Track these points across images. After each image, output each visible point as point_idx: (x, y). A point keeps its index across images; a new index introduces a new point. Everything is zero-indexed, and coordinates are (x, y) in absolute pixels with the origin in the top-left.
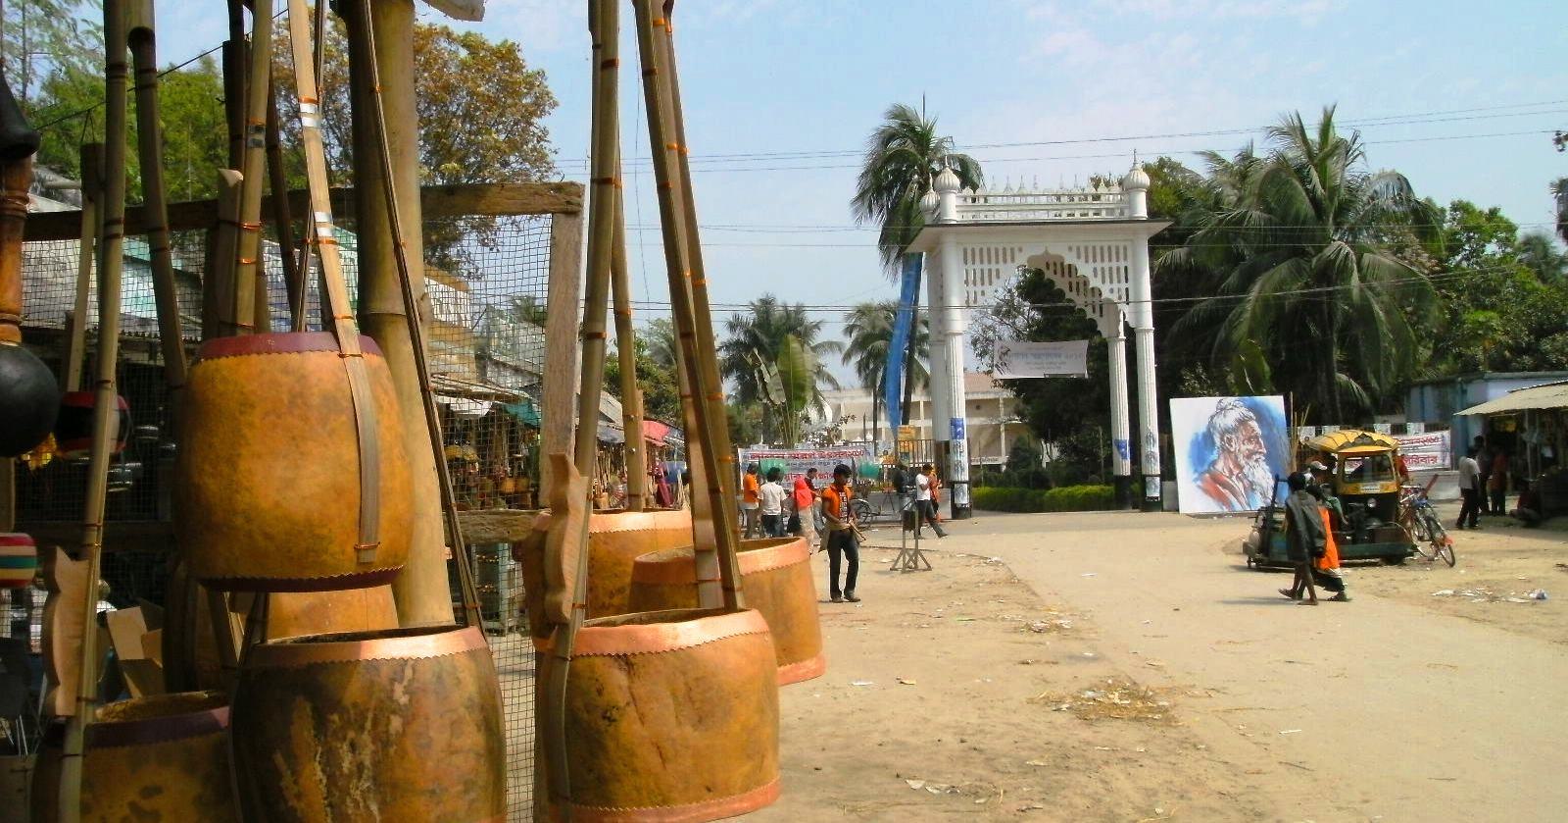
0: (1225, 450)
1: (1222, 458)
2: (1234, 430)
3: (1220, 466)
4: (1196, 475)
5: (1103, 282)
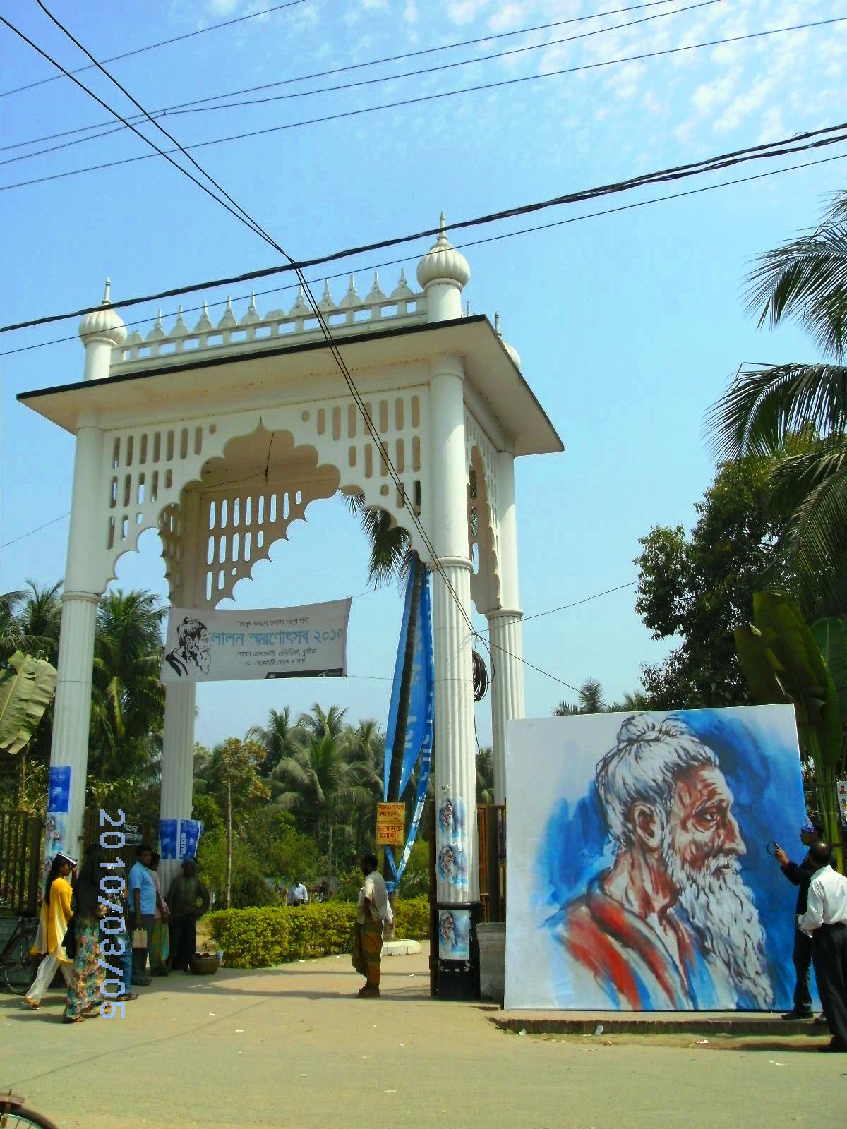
0: (635, 846)
1: (625, 863)
2: (662, 792)
3: (618, 886)
4: (554, 910)
5: (368, 474)
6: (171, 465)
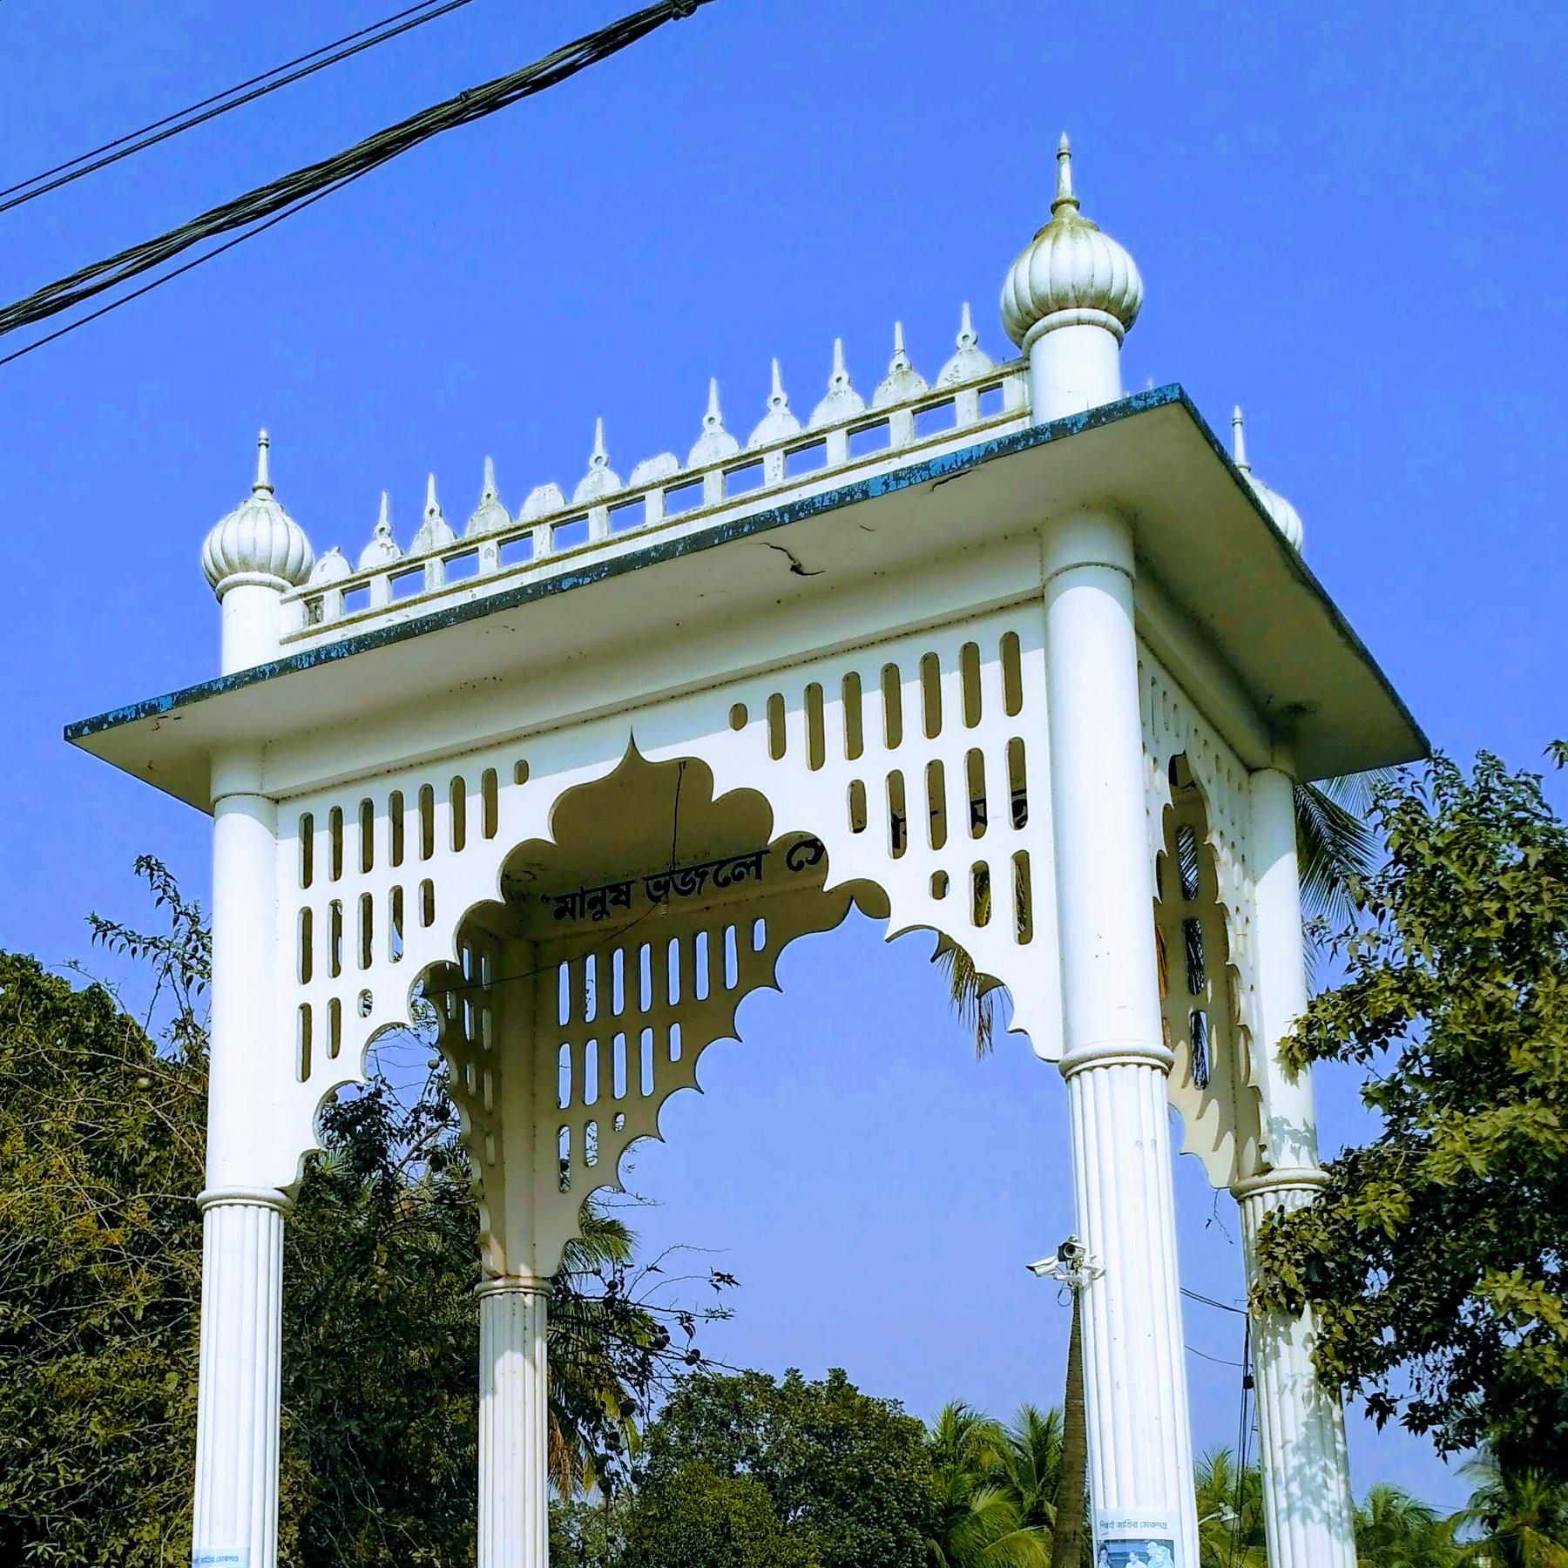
6: (429, 869)
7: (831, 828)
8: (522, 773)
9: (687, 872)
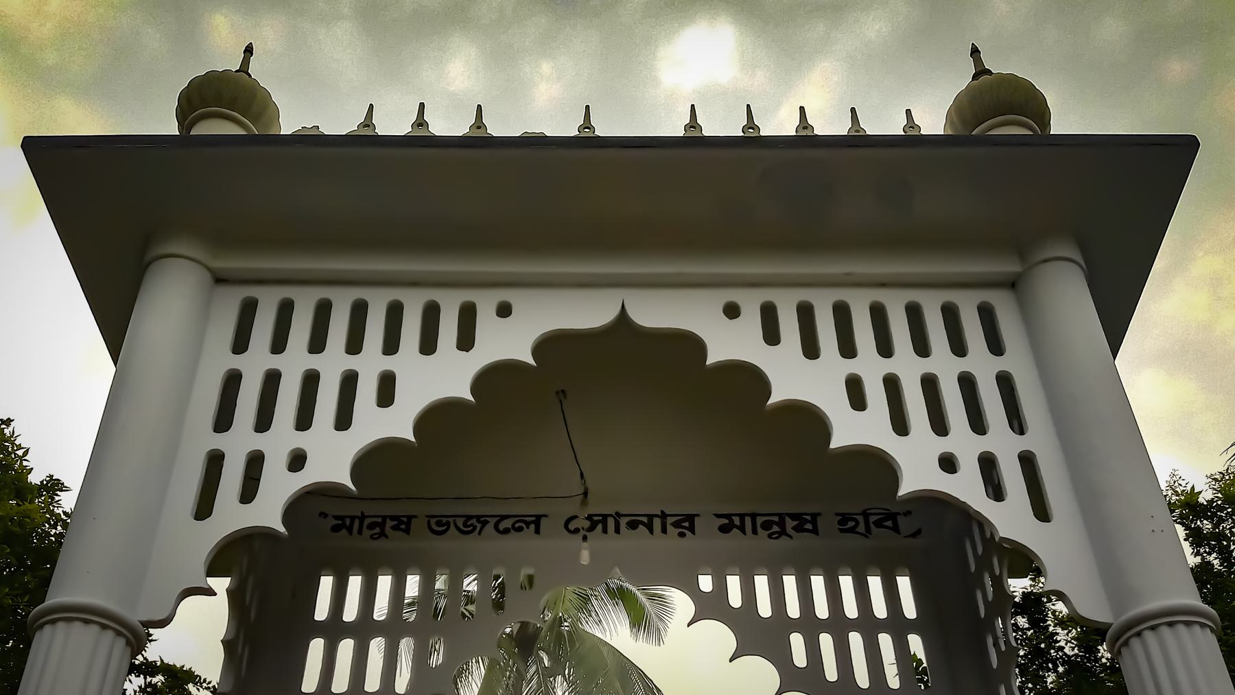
7: (834, 405)
8: (504, 311)
9: (469, 517)
